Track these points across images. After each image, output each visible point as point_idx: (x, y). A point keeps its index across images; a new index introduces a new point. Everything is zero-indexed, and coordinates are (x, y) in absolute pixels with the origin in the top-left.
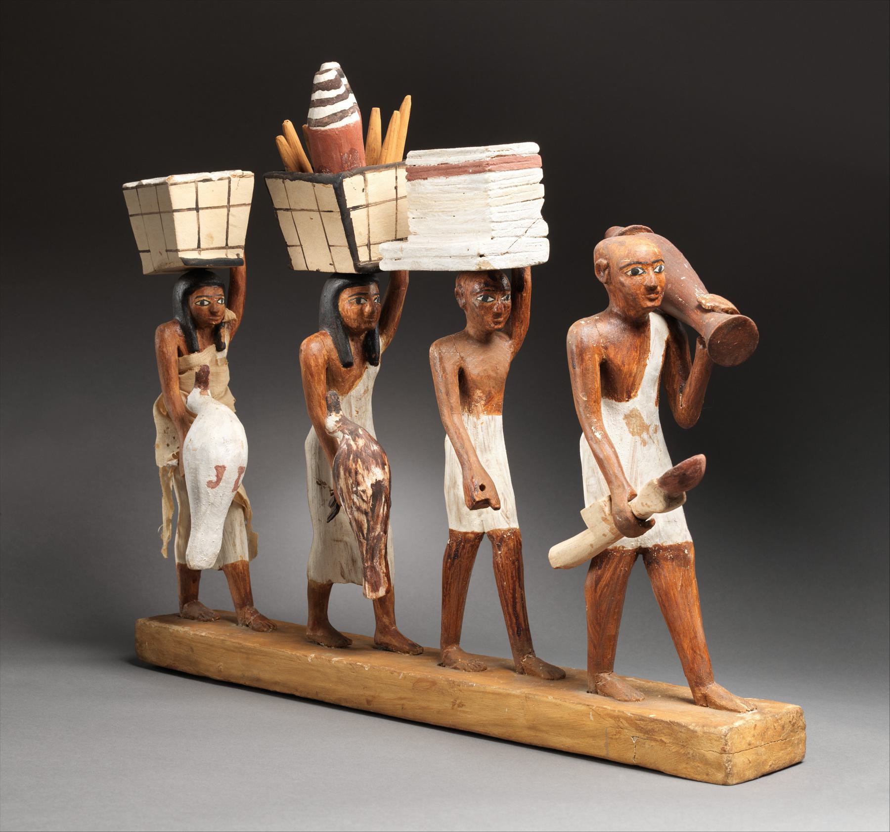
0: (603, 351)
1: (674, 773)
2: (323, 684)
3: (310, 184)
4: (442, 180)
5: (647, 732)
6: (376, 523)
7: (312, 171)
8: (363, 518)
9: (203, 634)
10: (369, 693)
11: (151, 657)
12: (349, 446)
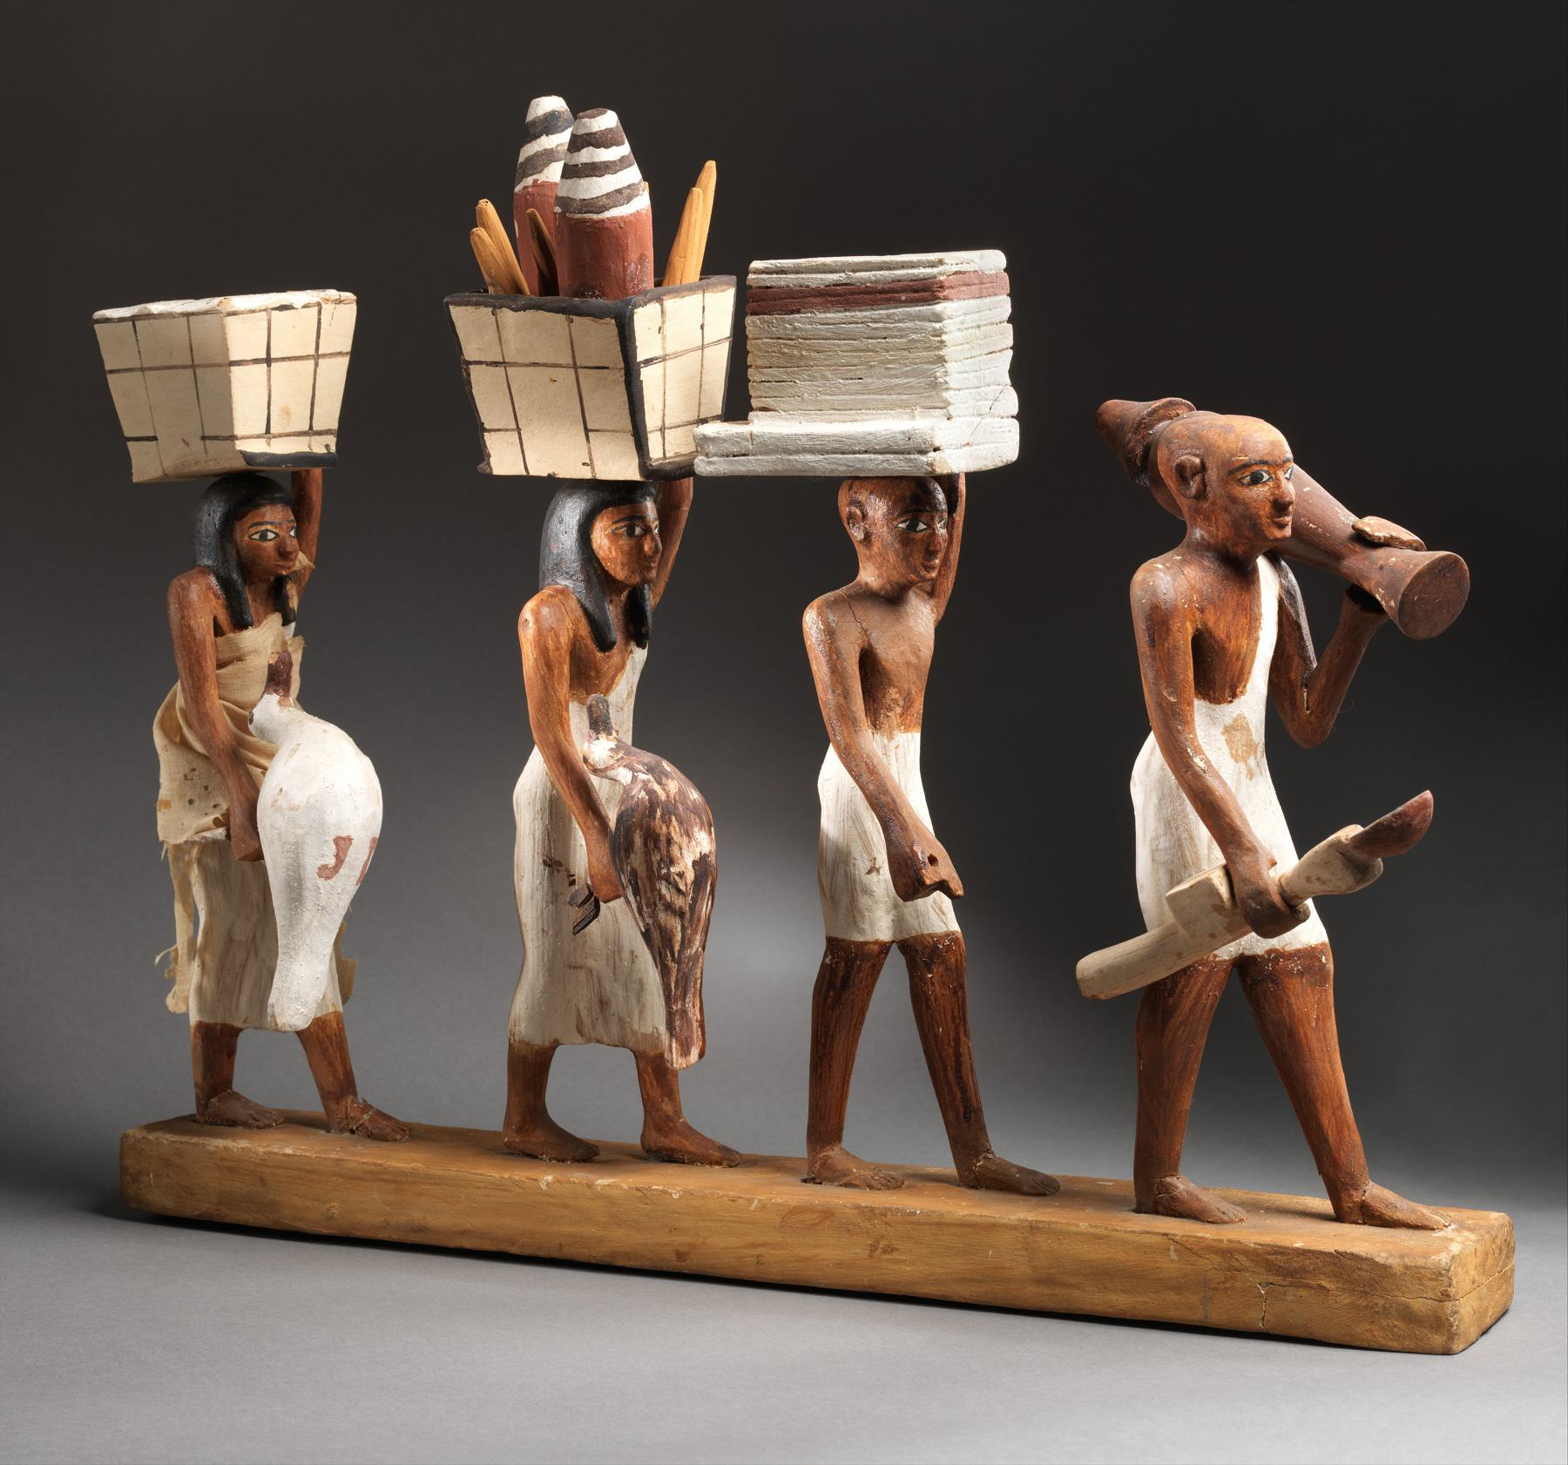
0: (1198, 614)
1: (1347, 1340)
2: (574, 1229)
3: (561, 317)
5: (1290, 1273)
6: (695, 932)
9: (289, 1151)
10: (679, 1239)
11: (160, 1199)
12: (651, 792)
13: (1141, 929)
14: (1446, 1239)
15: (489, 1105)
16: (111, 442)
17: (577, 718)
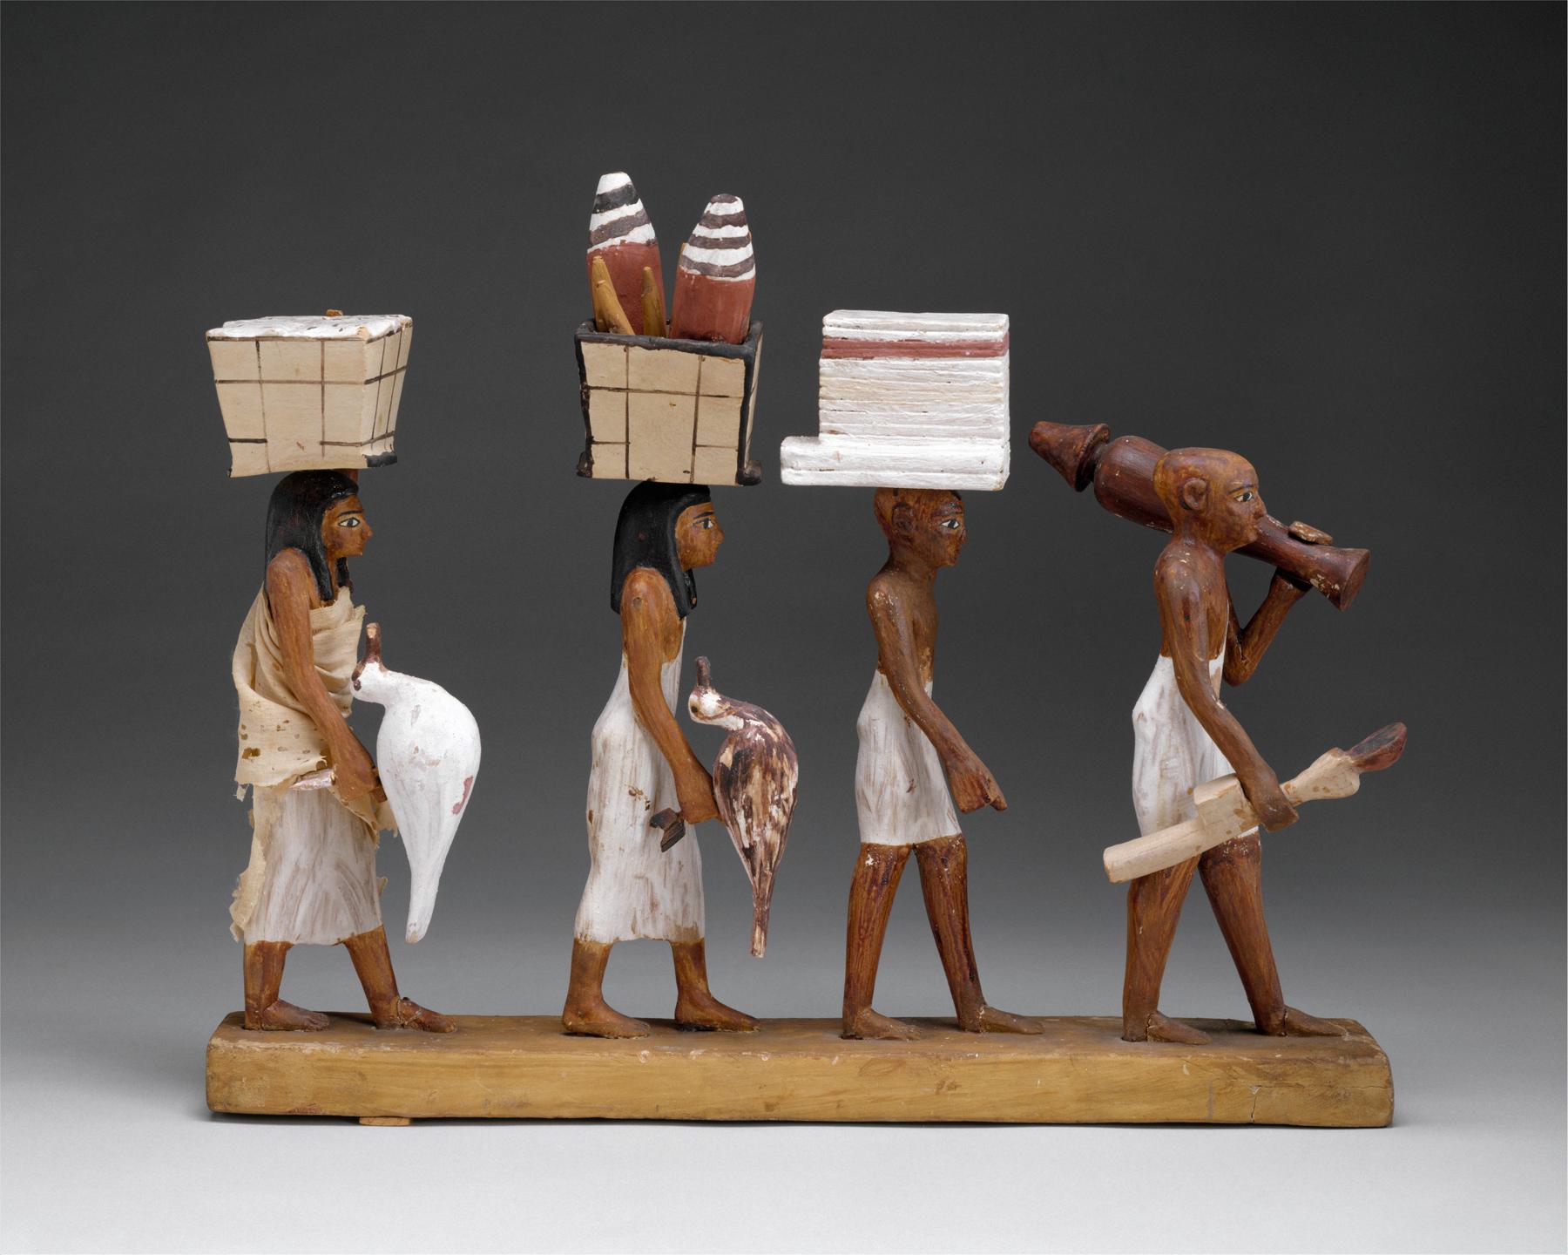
7: (631, 332)
12: (765, 735)
16: (219, 444)
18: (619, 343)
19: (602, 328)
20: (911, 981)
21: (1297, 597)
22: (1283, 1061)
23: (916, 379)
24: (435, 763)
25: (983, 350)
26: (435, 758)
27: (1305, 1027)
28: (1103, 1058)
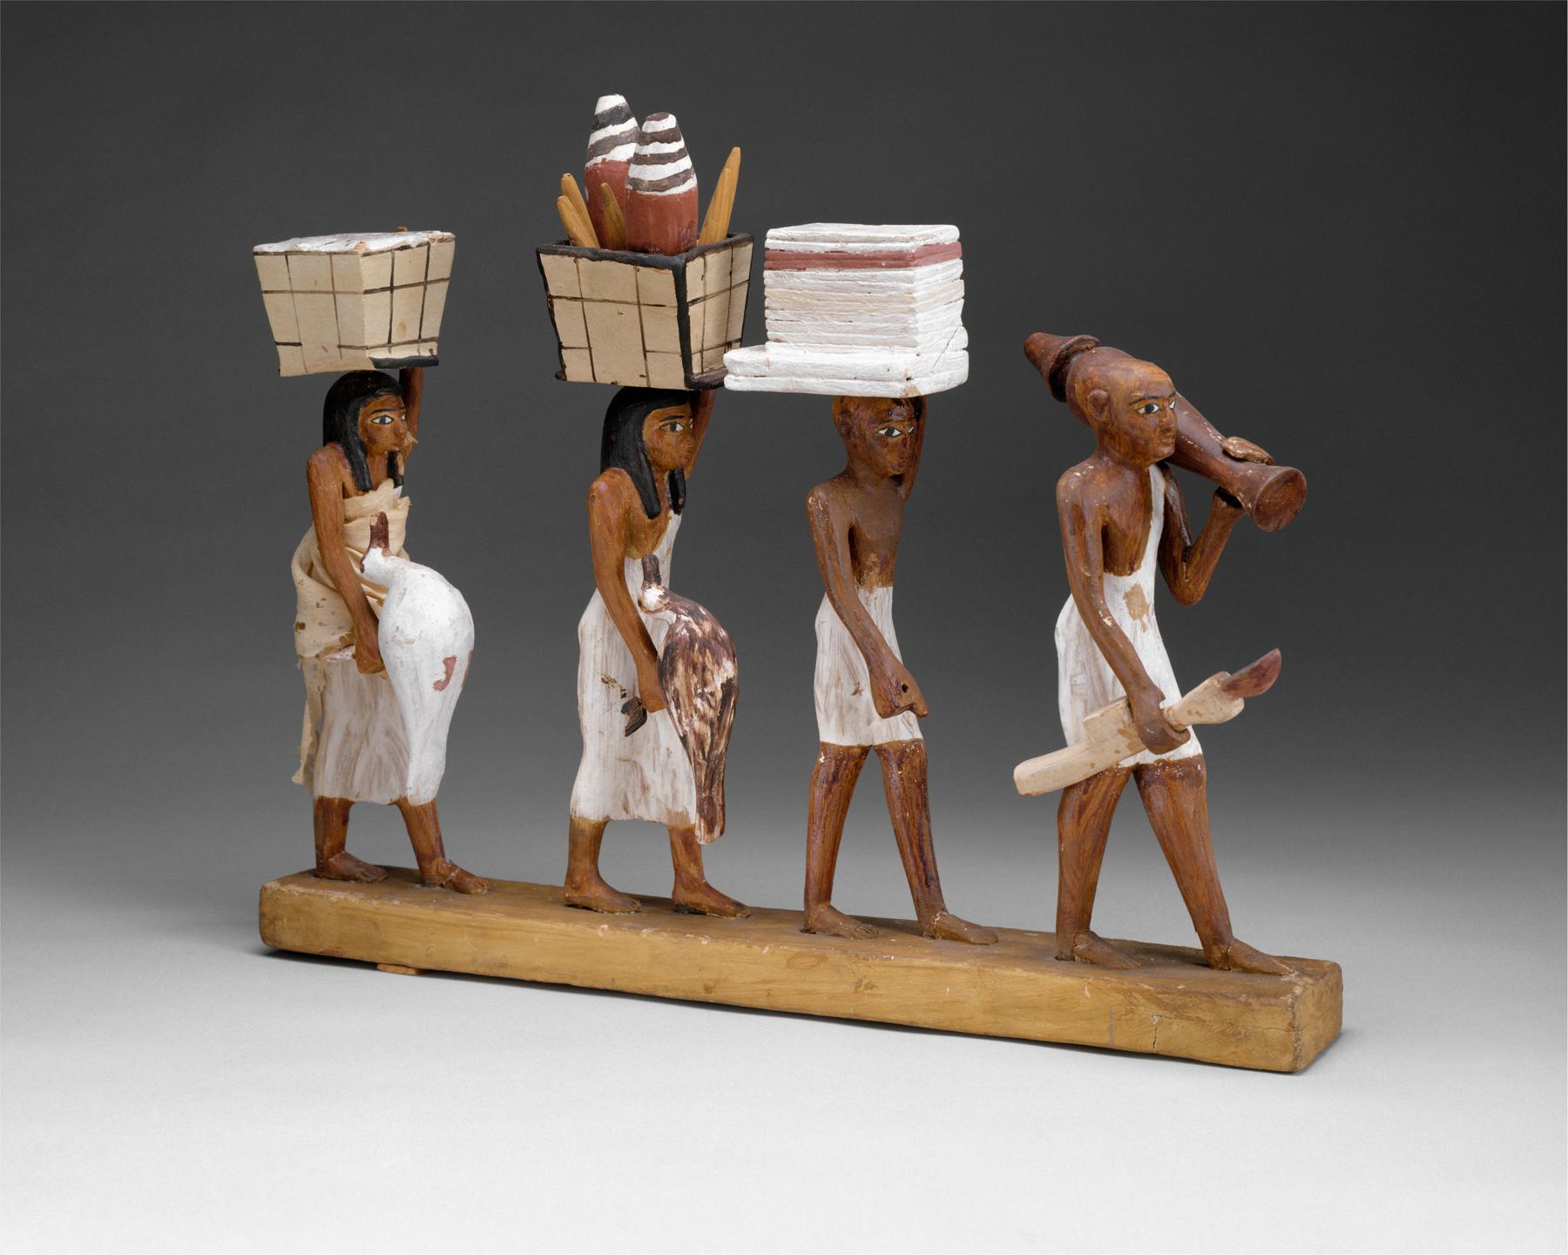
3: (630, 267)
4: (832, 273)
8: (706, 730)
12: (691, 631)
13: (1059, 742)
14: (1290, 982)
15: (553, 870)
16: (265, 345)
17: (634, 574)
18: (570, 255)
19: (566, 244)
20: (872, 882)
21: (1235, 516)
22: (1184, 993)
23: (841, 290)
24: (411, 642)
25: (932, 253)
26: (411, 637)
27: (1247, 963)
28: (1009, 973)
